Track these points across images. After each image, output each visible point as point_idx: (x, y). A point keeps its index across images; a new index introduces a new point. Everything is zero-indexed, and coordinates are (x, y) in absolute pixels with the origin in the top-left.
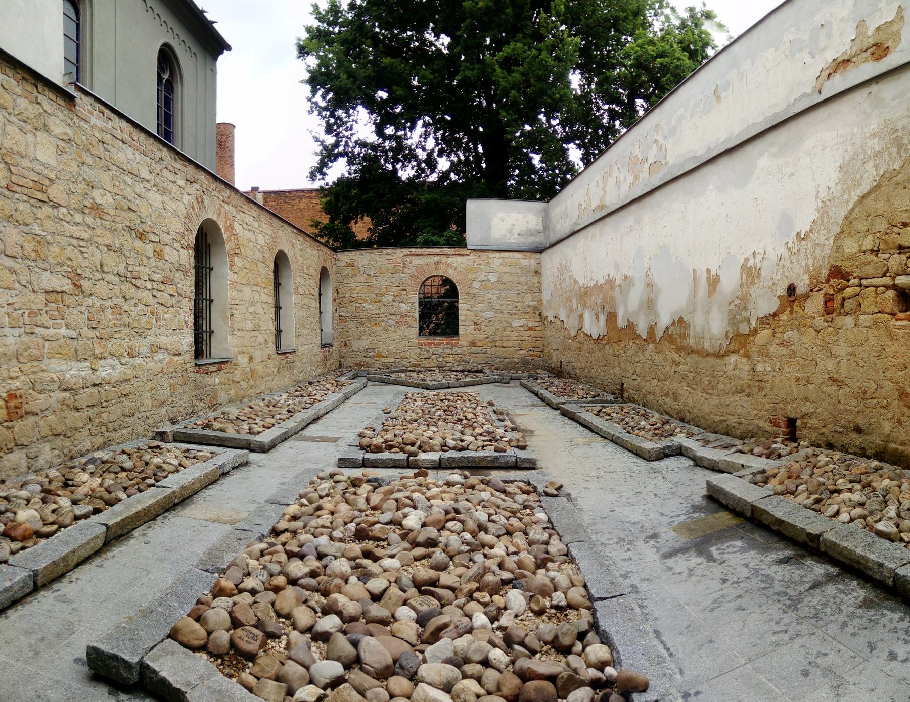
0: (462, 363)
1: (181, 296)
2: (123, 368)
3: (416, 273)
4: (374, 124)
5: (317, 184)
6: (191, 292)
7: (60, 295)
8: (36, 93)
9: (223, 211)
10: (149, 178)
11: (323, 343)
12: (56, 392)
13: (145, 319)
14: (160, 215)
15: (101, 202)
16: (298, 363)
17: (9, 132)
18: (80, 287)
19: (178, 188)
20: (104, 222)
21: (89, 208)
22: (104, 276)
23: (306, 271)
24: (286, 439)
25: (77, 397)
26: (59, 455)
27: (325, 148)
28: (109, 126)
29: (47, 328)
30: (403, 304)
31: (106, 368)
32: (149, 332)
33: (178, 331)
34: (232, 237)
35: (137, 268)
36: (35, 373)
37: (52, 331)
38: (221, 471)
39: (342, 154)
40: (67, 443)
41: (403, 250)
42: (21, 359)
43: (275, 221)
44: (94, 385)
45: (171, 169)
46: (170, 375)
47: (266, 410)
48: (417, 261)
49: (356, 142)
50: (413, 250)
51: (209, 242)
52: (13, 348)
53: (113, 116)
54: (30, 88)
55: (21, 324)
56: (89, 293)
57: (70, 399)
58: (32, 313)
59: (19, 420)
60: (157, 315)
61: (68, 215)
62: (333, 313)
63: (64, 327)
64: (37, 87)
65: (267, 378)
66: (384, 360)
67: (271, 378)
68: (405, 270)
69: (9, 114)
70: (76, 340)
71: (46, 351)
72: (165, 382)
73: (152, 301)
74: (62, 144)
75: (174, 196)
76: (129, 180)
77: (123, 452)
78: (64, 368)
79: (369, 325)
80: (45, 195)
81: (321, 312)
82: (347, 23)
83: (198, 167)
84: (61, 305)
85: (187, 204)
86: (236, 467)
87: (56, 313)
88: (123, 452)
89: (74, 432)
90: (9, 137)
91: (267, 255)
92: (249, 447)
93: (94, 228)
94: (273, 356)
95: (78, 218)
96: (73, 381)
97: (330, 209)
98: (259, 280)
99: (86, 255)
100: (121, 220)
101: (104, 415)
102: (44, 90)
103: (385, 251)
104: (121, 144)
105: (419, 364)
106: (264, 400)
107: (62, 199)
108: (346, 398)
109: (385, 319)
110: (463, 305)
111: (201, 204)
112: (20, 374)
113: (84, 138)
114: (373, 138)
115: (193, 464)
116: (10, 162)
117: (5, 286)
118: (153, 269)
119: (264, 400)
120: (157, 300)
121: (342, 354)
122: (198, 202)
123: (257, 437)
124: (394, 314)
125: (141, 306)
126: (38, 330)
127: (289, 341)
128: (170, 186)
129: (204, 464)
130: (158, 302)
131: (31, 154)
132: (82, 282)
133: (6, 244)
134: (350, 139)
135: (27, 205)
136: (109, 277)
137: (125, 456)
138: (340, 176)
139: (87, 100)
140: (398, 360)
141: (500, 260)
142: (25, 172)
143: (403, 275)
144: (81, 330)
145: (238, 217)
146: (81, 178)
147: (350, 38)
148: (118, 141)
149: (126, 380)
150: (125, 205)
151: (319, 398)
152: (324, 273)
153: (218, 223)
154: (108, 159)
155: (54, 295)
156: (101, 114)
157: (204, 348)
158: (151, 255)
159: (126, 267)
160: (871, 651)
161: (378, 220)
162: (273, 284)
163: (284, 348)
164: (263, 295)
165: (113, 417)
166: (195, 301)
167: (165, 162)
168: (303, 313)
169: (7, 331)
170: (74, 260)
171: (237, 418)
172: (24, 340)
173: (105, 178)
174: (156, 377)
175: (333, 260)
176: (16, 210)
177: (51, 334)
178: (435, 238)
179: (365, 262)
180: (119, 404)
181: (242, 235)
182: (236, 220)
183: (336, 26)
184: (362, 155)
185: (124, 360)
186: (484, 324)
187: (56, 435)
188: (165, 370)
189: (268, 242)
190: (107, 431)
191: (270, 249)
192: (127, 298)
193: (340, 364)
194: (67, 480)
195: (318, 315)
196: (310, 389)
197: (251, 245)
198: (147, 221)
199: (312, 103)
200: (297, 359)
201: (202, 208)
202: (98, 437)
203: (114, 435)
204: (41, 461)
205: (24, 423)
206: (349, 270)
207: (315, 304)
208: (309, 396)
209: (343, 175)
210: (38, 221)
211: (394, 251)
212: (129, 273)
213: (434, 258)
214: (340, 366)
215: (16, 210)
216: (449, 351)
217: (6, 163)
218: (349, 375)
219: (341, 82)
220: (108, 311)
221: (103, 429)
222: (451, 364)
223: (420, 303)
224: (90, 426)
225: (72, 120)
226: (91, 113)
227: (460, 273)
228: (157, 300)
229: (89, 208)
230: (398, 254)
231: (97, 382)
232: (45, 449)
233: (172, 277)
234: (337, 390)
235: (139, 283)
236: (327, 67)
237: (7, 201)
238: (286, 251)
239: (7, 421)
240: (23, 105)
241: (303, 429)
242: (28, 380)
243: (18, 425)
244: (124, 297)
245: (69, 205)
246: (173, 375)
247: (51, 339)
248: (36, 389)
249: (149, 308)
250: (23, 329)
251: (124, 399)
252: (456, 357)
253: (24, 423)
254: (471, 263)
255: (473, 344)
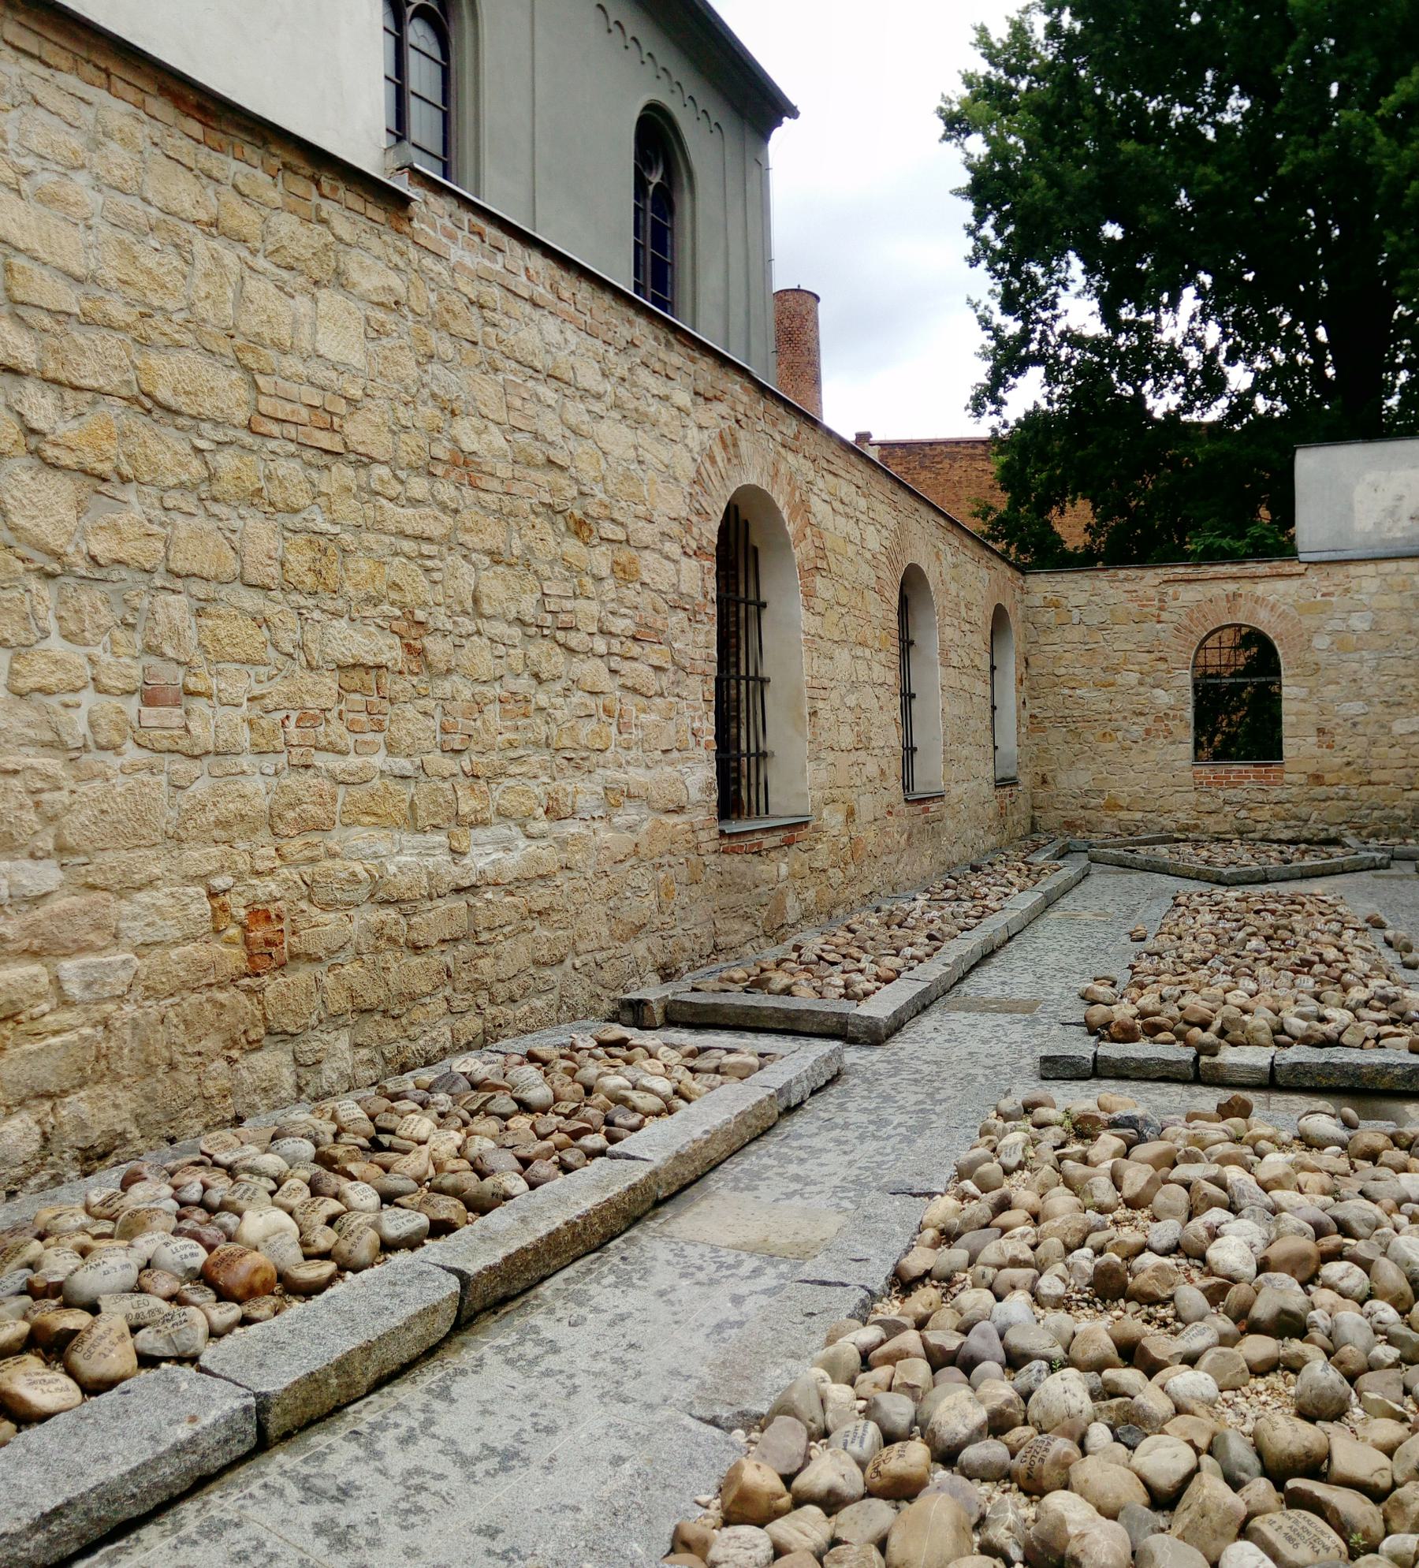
0: (1292, 823)
1: (684, 669)
2: (533, 847)
3: (1186, 622)
4: (1096, 296)
5: (981, 428)
6: (708, 660)
7: (373, 673)
8: (315, 199)
9: (783, 469)
10: (601, 389)
11: (998, 777)
12: (362, 908)
13: (591, 725)
14: (627, 477)
15: (474, 447)
16: (949, 823)
17: (253, 296)
18: (421, 653)
19: (675, 412)
20: (481, 494)
21: (445, 462)
22: (484, 625)
23: (964, 614)
24: (925, 1007)
25: (415, 920)
26: (371, 1061)
27: (1001, 343)
28: (498, 267)
29: (340, 752)
30: (1159, 692)
31: (489, 848)
32: (601, 758)
33: (675, 754)
34: (808, 531)
35: (568, 605)
36: (313, 860)
37: (353, 761)
38: (783, 1103)
39: (1037, 359)
40: (391, 1031)
41: (1160, 571)
42: (281, 827)
43: (902, 497)
44: (458, 890)
45: (658, 366)
46: (657, 860)
47: (882, 935)
48: (1189, 594)
49: (1063, 334)
50: (1181, 571)
51: (755, 539)
52: (263, 803)
53: (505, 241)
54: (301, 187)
55: (279, 744)
56: (443, 667)
57: (397, 923)
58: (307, 720)
59: (276, 974)
60: (621, 716)
61: (394, 482)
62: (1018, 711)
63: (383, 751)
64: (318, 184)
65: (885, 859)
66: (1123, 815)
67: (893, 858)
68: (1165, 616)
69: (254, 252)
70: (412, 782)
71: (338, 807)
72: (642, 878)
73: (607, 683)
74: (379, 315)
75: (665, 431)
76: (547, 393)
77: (532, 1058)
78: (382, 848)
79: (1091, 738)
80: (338, 438)
81: (994, 708)
82: (1047, 70)
83: (724, 362)
84: (375, 699)
85: (697, 449)
86: (820, 1089)
87: (364, 717)
88: (532, 1058)
89: (410, 1004)
90: (252, 308)
91: (885, 574)
92: (841, 1031)
93: (456, 511)
94: (897, 808)
95: (419, 487)
96: (404, 881)
97: (1011, 479)
98: (868, 631)
99: (436, 576)
100: (527, 489)
101: (485, 964)
102: (335, 189)
103: (1122, 574)
104: (528, 308)
105: (1196, 826)
106: (878, 910)
107: (378, 444)
108: (1049, 902)
109: (1124, 724)
110: (1291, 691)
111: (731, 450)
112: (278, 863)
113: (433, 297)
114: (1095, 328)
115: (712, 1088)
116: (254, 366)
117: (243, 657)
118: (611, 606)
119: (878, 910)
120: (621, 681)
121: (1038, 803)
122: (725, 447)
123: (863, 1004)
124: (1141, 714)
125: (578, 697)
126: (321, 760)
127: (930, 773)
128: (654, 408)
129: (740, 1086)
130: (624, 687)
131: (306, 345)
132: (428, 642)
133: (247, 559)
134: (1051, 327)
135: (295, 464)
136: (499, 628)
137: (531, 1071)
138: (1030, 408)
139: (440, 205)
140: (1150, 816)
141: (1377, 581)
142: (292, 389)
143: (1159, 626)
144: (426, 757)
145: (820, 484)
146: (426, 392)
147: (1050, 102)
148: (521, 303)
149: (541, 877)
150: (539, 455)
151: (994, 905)
152: (1000, 617)
153: (774, 496)
154: (494, 344)
155: (358, 676)
156: (476, 239)
157: (744, 794)
158: (605, 572)
159: (541, 603)
160: (1161, 997)
161: (1107, 506)
162: (896, 642)
163: (920, 789)
164: (876, 667)
165: (506, 968)
166: (718, 681)
167: (643, 351)
168: (959, 709)
169: (245, 762)
170: (407, 588)
171: (820, 958)
172: (288, 782)
173: (488, 390)
174: (620, 866)
175: (1018, 591)
176: (269, 478)
177: (352, 767)
178: (1225, 542)
179: (1080, 599)
180: (524, 937)
181: (830, 526)
182: (815, 490)
183: (1023, 77)
184: (1074, 363)
185: (535, 827)
186: (1340, 730)
187: (363, 1011)
188: (643, 850)
189: (887, 543)
190: (492, 1002)
191: (891, 562)
192: (543, 676)
193: (1033, 824)
194: (381, 1130)
195: (989, 714)
196: (973, 883)
197: (851, 550)
198: (596, 492)
199: (977, 239)
200: (947, 812)
201: (735, 461)
202: (469, 1016)
203: (510, 1012)
204: (328, 1073)
205: (289, 980)
206: (1049, 617)
207: (982, 689)
208: (973, 898)
209: (1036, 405)
210: (321, 500)
211: (1139, 573)
212: (549, 617)
213: (1225, 586)
214: (1034, 829)
215: (269, 478)
216: (1260, 797)
217: (247, 369)
218: (1053, 849)
219: (1035, 193)
220: (493, 711)
221: (483, 998)
222: (1266, 825)
223: (1196, 687)
224: (448, 991)
225: (402, 254)
226: (451, 237)
227: (1283, 616)
228: (621, 681)
229: (445, 462)
230: (1150, 579)
231: (466, 883)
232: (338, 1045)
233: (659, 625)
234: (1030, 883)
235: (573, 640)
236: (1005, 161)
237: (248, 458)
238: (925, 569)
239: (247, 975)
240: (284, 230)
241: (961, 980)
242: (297, 878)
243: (273, 985)
244: (536, 676)
245: (394, 459)
246: (664, 861)
247: (351, 779)
248: (315, 899)
249: (600, 701)
250: (285, 755)
251: (536, 923)
252: (1278, 808)
253: (289, 980)
254: (1306, 593)
255: (1317, 779)
